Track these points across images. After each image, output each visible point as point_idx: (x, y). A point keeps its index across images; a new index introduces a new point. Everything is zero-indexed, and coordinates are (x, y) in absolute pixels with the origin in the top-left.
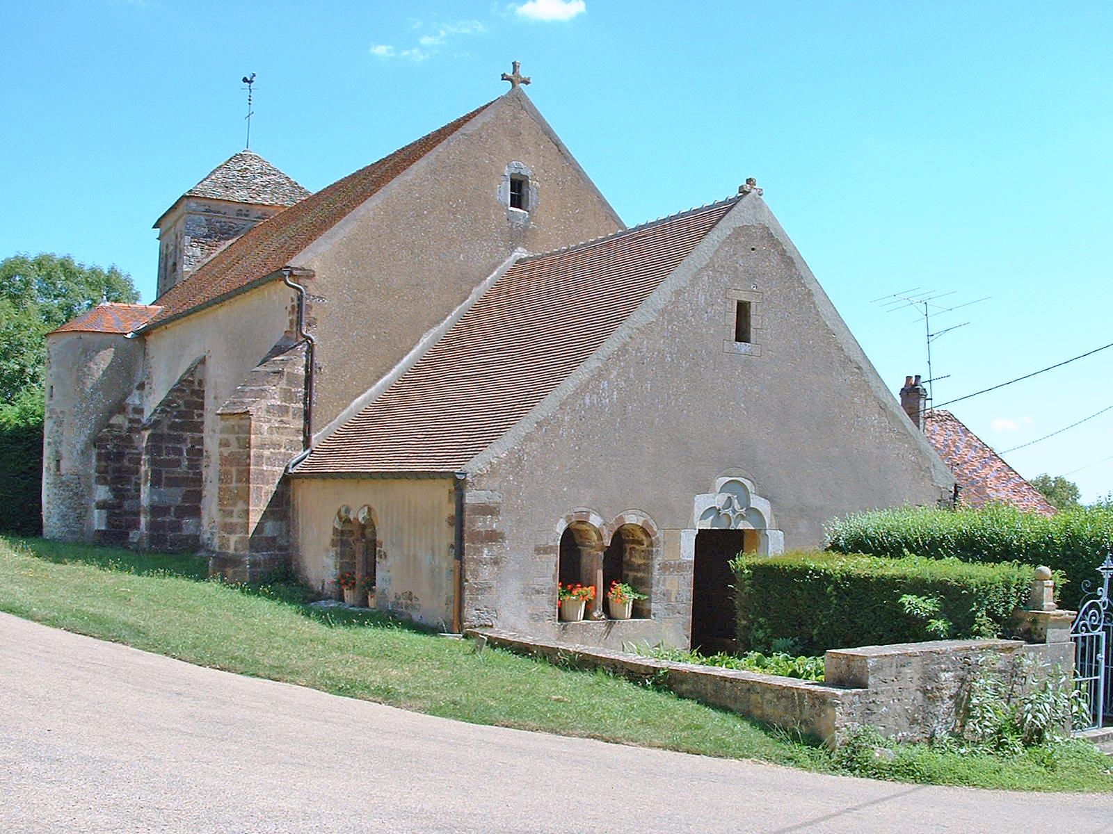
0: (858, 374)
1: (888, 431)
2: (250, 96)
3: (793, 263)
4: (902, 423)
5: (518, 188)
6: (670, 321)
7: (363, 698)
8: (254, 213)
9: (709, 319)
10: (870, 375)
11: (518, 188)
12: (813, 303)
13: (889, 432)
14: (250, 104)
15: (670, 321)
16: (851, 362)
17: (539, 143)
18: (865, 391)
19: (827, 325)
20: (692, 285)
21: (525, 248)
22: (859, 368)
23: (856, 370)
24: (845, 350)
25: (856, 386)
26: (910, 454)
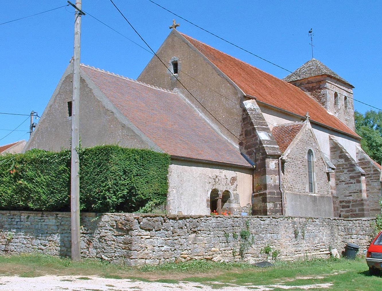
0: (112, 115)
1: (126, 136)
2: (311, 38)
3: (85, 81)
4: (133, 131)
5: (175, 65)
6: (49, 117)
7: (92, 274)
8: (297, 84)
9: (59, 112)
10: (117, 114)
11: (175, 65)
12: (92, 93)
13: (127, 136)
14: (312, 41)
15: (49, 117)
16: (109, 111)
17: (181, 46)
18: (115, 121)
19: (98, 100)
20: (54, 103)
21: (177, 87)
22: (112, 112)
23: (111, 114)
24: (106, 107)
25: (111, 120)
26: (138, 144)
